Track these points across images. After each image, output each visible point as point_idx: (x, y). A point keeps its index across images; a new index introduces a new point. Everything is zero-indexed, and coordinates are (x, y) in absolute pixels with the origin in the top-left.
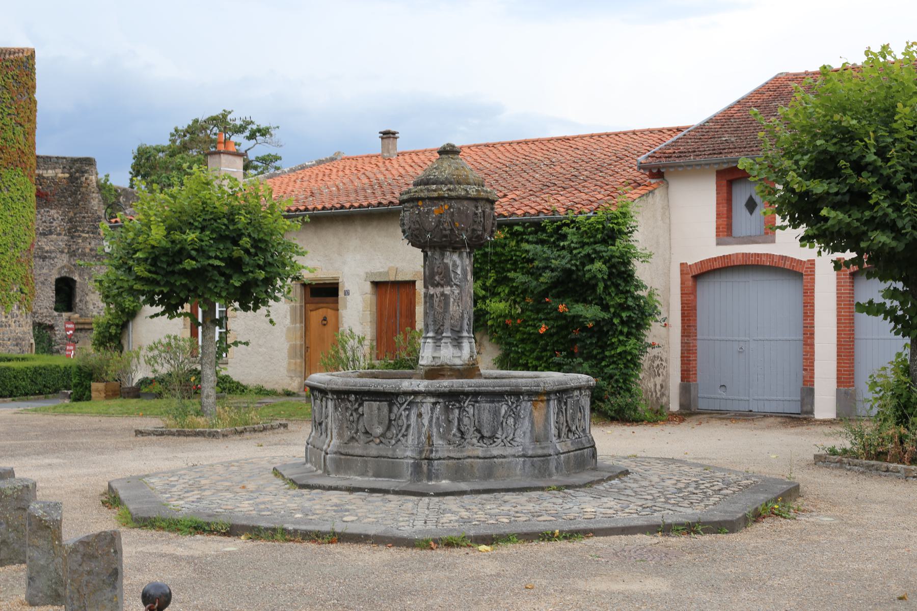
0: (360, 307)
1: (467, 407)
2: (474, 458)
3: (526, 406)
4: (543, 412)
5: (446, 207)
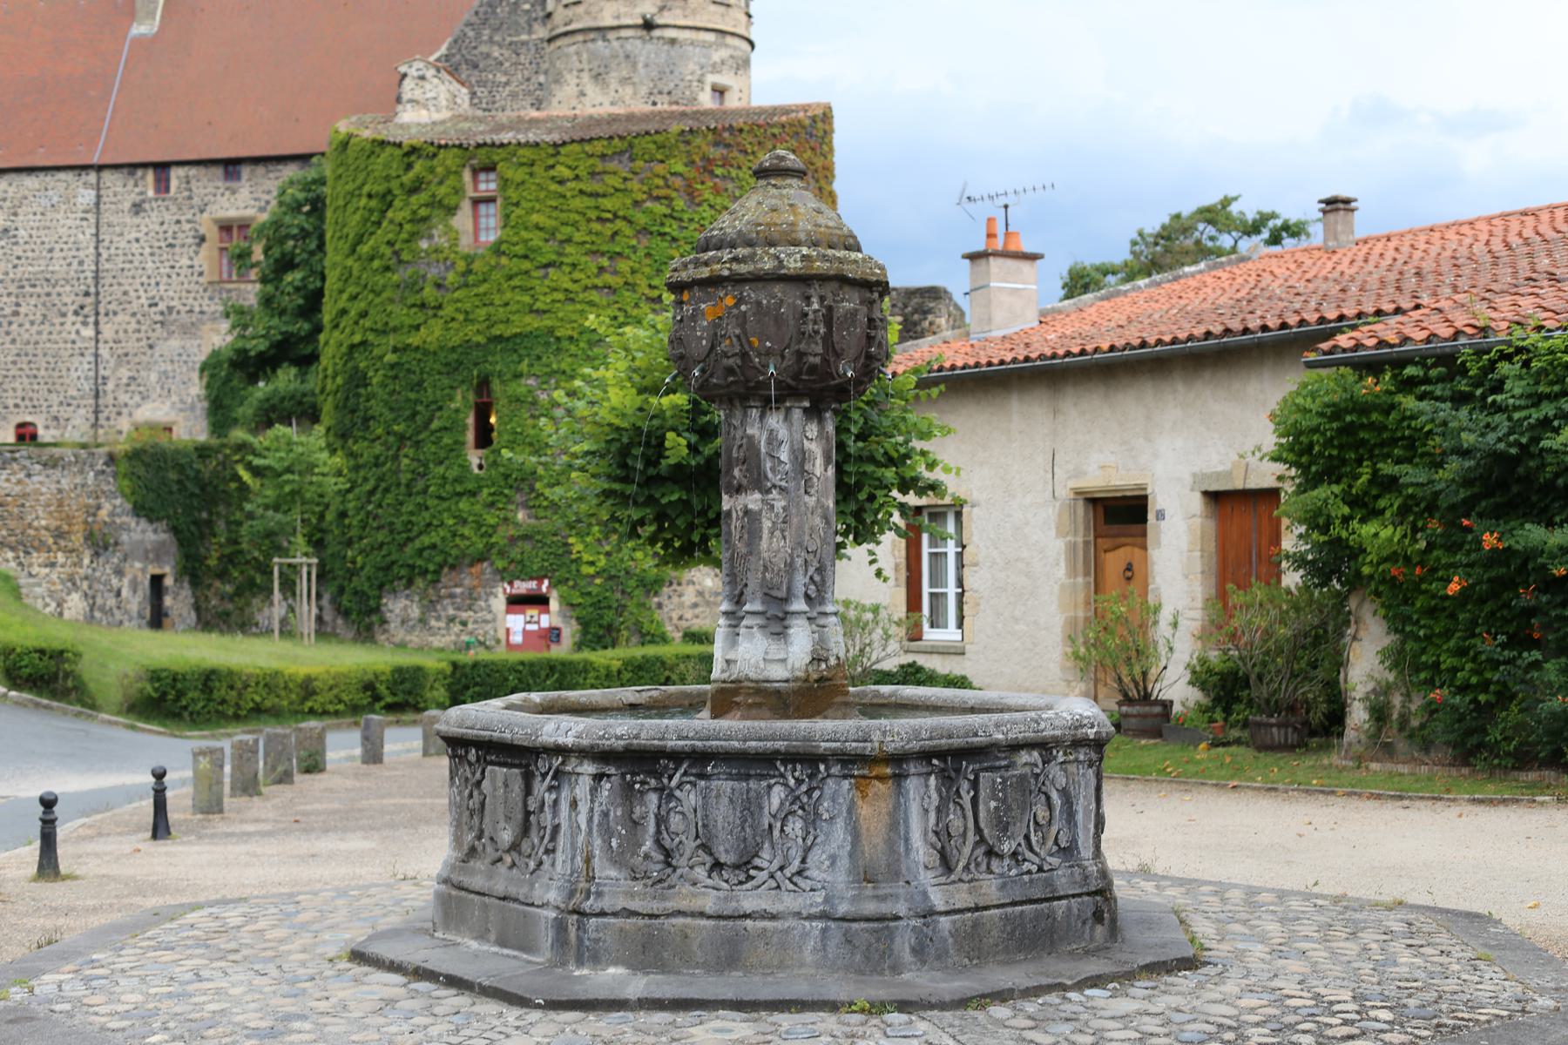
0: (1184, 545)
1: (680, 786)
2: (693, 915)
3: (837, 790)
4: (884, 806)
5: (729, 301)
